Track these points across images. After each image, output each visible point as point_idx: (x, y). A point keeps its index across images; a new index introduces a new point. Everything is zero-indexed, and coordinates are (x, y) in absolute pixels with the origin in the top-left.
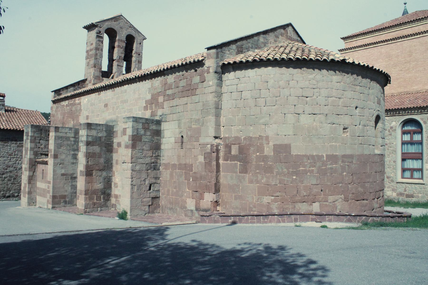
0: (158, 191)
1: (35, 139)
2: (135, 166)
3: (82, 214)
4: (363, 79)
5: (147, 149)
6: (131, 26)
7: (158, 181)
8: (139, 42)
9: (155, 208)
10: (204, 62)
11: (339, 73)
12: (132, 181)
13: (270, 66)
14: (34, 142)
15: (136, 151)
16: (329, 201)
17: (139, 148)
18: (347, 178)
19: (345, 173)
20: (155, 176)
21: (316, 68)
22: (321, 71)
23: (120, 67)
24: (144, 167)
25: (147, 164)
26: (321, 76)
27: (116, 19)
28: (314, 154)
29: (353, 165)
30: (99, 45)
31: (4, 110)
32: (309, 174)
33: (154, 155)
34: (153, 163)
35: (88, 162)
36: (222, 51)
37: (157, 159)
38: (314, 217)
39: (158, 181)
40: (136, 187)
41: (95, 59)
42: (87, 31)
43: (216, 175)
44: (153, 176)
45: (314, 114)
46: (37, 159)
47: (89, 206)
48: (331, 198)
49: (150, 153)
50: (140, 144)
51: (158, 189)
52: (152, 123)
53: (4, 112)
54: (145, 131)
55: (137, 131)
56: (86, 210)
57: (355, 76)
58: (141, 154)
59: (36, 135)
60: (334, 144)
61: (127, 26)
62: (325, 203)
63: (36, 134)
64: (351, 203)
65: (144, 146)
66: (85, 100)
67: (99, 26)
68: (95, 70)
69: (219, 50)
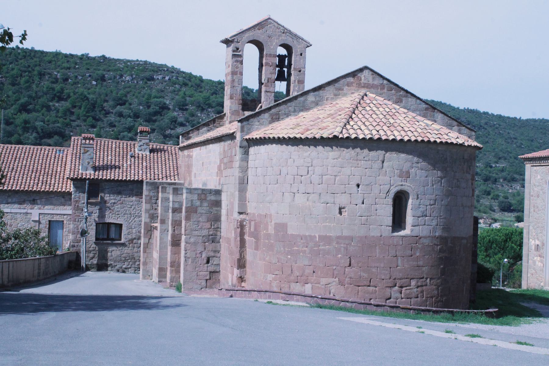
0: (218, 265)
1: (151, 198)
2: (190, 238)
3: (168, 288)
4: (371, 152)
5: (203, 221)
6: (285, 31)
7: (218, 255)
8: (299, 53)
9: (214, 283)
10: (235, 134)
11: (337, 149)
12: (186, 254)
13: (274, 143)
14: (149, 203)
15: (191, 223)
16: (321, 283)
17: (194, 220)
18: (343, 261)
19: (340, 256)
20: (214, 249)
21: (312, 145)
22: (316, 147)
23: (269, 93)
24: (200, 240)
25: (204, 236)
26: (317, 153)
27: (260, 25)
28: (307, 234)
29: (352, 247)
30: (236, 67)
31: (149, 150)
32: (301, 254)
33: (212, 227)
34: (212, 235)
35: (174, 231)
36: (248, 124)
37: (217, 231)
38: (284, 295)
39: (218, 255)
40: (190, 259)
41: (231, 88)
42: (225, 45)
43: (240, 251)
44: (211, 249)
45: (308, 193)
46: (154, 223)
47: (175, 280)
48: (324, 281)
49: (208, 225)
50: (194, 216)
51: (217, 263)
52: (210, 193)
53: (148, 153)
54: (201, 202)
55: (192, 202)
56: (171, 283)
57: (358, 150)
58: (197, 226)
59: (151, 194)
60: (327, 224)
61: (278, 32)
62: (317, 285)
63: (152, 193)
64: (349, 288)
65: (199, 218)
66: (195, 152)
67: (236, 40)
68: (232, 103)
69: (245, 123)
